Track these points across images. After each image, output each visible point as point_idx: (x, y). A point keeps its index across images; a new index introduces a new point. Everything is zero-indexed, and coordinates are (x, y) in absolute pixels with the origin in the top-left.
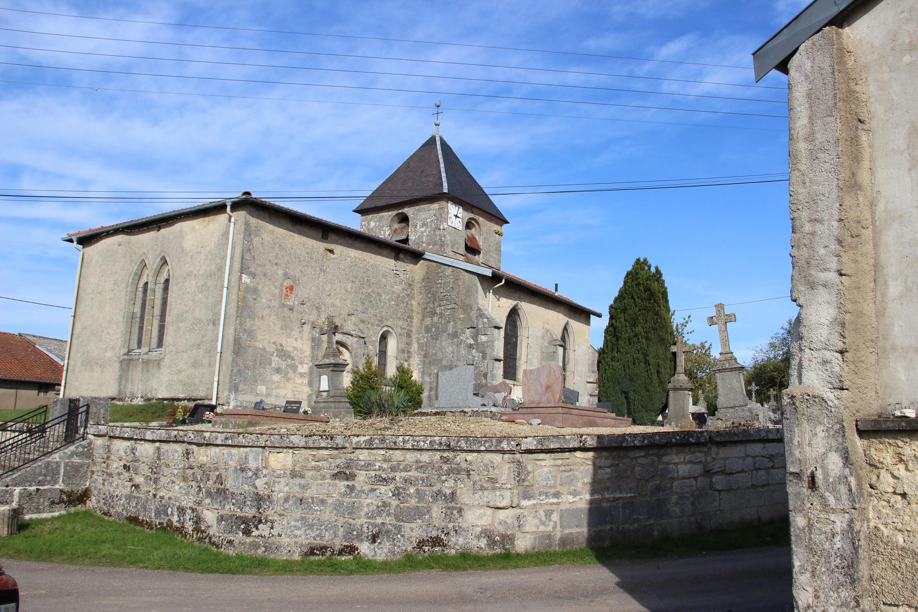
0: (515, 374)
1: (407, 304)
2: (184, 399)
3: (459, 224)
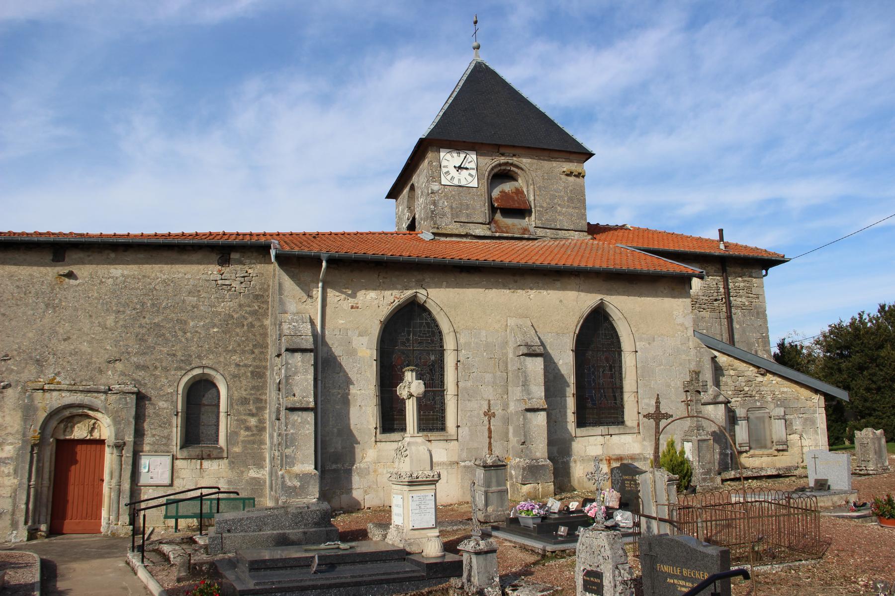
0: (443, 419)
1: (252, 325)
2: (657, 441)
3: (469, 179)
